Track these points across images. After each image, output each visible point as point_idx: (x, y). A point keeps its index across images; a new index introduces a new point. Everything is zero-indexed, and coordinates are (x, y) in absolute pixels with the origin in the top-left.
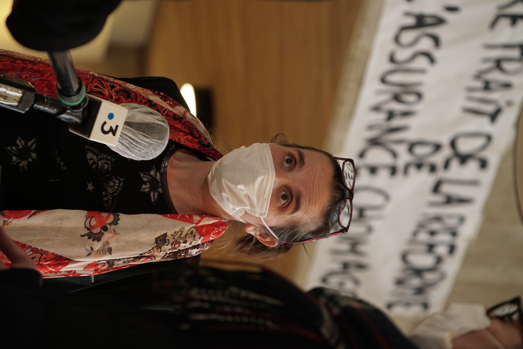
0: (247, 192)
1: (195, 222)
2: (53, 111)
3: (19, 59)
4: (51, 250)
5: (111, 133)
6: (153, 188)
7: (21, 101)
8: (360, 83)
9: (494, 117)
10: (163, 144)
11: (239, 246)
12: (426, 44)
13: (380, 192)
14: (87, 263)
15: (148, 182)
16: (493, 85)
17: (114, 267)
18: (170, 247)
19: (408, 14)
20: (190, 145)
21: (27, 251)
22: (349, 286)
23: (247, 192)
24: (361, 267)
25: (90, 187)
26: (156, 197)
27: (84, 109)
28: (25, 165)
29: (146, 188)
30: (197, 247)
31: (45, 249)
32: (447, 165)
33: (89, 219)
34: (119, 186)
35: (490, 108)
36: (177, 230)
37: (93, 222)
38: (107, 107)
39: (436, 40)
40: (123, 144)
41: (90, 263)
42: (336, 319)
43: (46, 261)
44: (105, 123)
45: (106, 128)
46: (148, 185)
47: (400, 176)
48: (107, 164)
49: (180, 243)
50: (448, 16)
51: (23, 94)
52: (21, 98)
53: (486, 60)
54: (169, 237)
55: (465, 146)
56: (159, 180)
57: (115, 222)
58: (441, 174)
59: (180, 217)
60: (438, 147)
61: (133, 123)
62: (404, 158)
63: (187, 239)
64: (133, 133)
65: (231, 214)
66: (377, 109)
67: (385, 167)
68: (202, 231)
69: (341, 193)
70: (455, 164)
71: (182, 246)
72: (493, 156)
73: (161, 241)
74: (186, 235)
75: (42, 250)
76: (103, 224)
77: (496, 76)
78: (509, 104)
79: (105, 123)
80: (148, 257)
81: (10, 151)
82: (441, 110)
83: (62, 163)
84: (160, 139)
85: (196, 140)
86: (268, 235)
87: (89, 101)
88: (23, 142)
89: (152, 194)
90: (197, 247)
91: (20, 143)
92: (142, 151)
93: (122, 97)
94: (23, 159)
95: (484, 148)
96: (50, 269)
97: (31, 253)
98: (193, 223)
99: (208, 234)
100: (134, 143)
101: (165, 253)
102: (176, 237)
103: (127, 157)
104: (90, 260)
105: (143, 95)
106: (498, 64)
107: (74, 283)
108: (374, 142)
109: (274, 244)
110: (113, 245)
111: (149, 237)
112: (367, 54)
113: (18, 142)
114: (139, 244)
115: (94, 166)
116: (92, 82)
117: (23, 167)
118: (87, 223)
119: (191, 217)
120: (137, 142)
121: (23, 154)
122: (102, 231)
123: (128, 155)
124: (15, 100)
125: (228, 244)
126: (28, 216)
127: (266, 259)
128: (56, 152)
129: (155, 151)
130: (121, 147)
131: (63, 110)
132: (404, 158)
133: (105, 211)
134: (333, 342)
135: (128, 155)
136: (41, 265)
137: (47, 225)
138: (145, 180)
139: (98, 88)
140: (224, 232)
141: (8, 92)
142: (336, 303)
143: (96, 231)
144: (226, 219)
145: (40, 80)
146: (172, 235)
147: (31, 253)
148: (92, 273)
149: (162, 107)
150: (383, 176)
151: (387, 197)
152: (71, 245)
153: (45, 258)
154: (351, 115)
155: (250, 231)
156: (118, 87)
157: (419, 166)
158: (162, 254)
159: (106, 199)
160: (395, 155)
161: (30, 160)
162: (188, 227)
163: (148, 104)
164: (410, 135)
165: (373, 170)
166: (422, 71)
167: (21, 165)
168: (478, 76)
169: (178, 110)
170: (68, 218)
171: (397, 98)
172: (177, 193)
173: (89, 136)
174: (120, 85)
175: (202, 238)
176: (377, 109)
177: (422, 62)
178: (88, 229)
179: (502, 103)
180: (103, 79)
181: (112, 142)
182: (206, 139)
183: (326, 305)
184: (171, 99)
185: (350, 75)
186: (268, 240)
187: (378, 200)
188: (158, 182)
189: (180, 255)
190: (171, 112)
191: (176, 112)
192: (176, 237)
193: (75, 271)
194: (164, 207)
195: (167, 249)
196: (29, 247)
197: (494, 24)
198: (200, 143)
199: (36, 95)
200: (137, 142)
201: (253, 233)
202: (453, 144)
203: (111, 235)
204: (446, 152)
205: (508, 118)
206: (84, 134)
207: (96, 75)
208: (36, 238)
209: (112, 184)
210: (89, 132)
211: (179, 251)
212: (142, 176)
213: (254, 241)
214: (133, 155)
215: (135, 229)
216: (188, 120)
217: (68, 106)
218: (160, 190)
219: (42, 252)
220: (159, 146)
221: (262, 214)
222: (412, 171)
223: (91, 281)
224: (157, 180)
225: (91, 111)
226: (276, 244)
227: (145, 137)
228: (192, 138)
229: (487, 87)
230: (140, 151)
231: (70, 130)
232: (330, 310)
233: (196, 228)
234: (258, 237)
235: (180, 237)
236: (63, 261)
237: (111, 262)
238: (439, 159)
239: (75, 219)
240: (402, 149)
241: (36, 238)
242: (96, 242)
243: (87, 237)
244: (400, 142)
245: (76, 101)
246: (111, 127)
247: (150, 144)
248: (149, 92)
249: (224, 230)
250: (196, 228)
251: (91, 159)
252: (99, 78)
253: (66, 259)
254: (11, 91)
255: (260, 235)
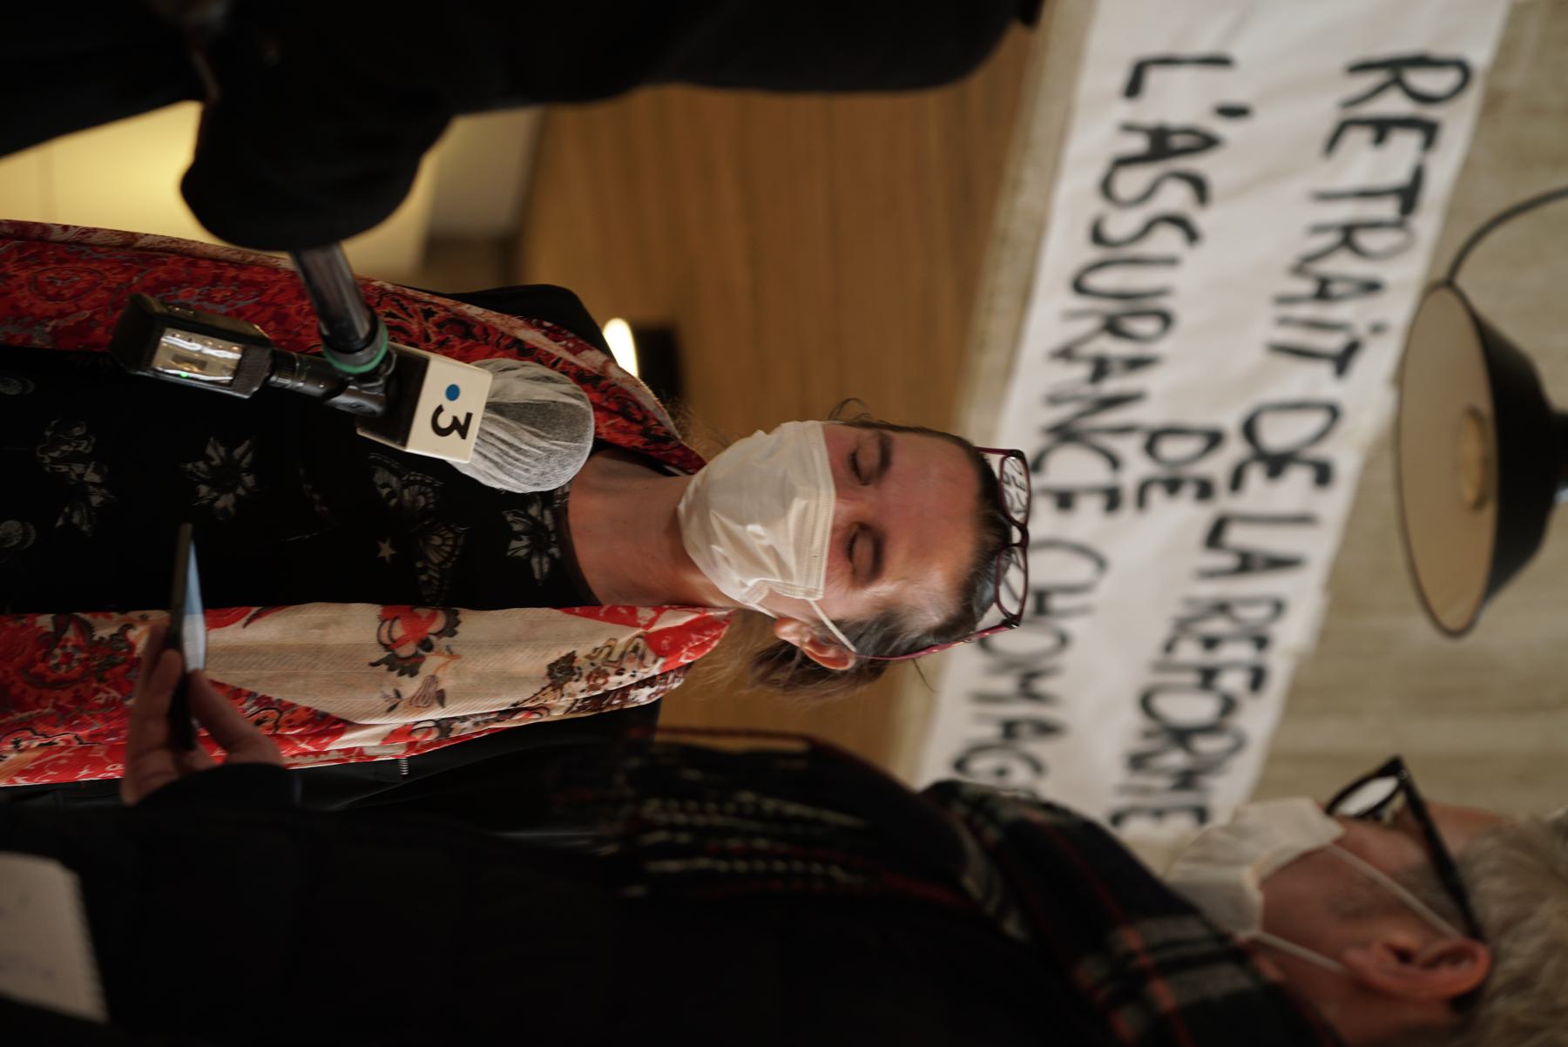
0: (772, 544)
1: (643, 622)
2: (316, 389)
3: (204, 257)
4: (303, 702)
5: (455, 434)
6: (539, 546)
7: (238, 369)
8: (1025, 296)
9: (1343, 361)
10: (580, 450)
11: (761, 670)
12: (1175, 197)
13: (1082, 550)
14: (388, 729)
15: (524, 533)
16: (1337, 289)
17: (453, 735)
18: (583, 684)
19: (1129, 128)
20: (622, 440)
21: (245, 705)
22: (1020, 776)
23: (772, 544)
24: (1046, 729)
25: (386, 551)
26: (546, 567)
27: (389, 380)
28: (230, 504)
29: (519, 547)
30: (650, 682)
31: (289, 699)
32: (1237, 480)
33: (387, 623)
34: (454, 547)
35: (1333, 342)
36: (600, 643)
37: (399, 631)
38: (441, 371)
39: (1199, 187)
40: (485, 457)
41: (395, 727)
42: (993, 854)
43: (292, 728)
44: (440, 410)
45: (444, 421)
46: (525, 541)
47: (1128, 510)
48: (424, 494)
49: (606, 675)
50: (1224, 129)
51: (244, 353)
52: (240, 361)
53: (1319, 229)
54: (581, 660)
55: (1279, 434)
56: (551, 528)
57: (450, 630)
58: (1225, 502)
59: (607, 613)
60: (1214, 439)
61: (506, 405)
62: (1137, 467)
63: (625, 665)
64: (507, 429)
65: (736, 598)
66: (1066, 354)
67: (1092, 490)
68: (661, 644)
69: (998, 534)
70: (1256, 477)
71: (614, 682)
72: (1345, 455)
73: (562, 671)
74: (622, 655)
75: (280, 701)
76: (420, 635)
77: (1343, 265)
78: (1378, 329)
79: (440, 410)
80: (532, 710)
81: (191, 473)
82: (1205, 370)
83: (316, 497)
84: (574, 440)
85: (635, 428)
86: (830, 641)
87: (399, 358)
88: (222, 450)
89: (535, 561)
90: (650, 682)
91: (216, 453)
92: (534, 471)
93: (469, 343)
94: (224, 490)
95: (1321, 436)
96: (303, 746)
97: (255, 709)
98: (638, 626)
99: (675, 649)
100: (512, 453)
101: (571, 699)
102: (598, 662)
103: (497, 486)
104: (396, 722)
105: (502, 329)
106: (1348, 236)
107: (361, 776)
108: (1064, 434)
109: (846, 664)
110: (447, 684)
111: (532, 663)
112: (1040, 227)
113: (210, 451)
114: (511, 680)
115: (393, 502)
116: (378, 305)
117: (225, 509)
118: (384, 632)
119: (633, 611)
120: (518, 450)
121: (224, 478)
122: (421, 652)
123: (501, 481)
124: (225, 368)
125: (731, 667)
126: (244, 620)
127: (827, 699)
128: (302, 471)
129: (564, 467)
130: (483, 465)
131: (340, 386)
132: (1137, 467)
133: (424, 605)
134: (991, 908)
135: (501, 481)
136: (281, 737)
137: (291, 640)
138: (517, 528)
139: (394, 316)
140: (715, 643)
141: (207, 351)
142: (991, 816)
143: (407, 650)
144: (721, 609)
145: (258, 303)
146: (588, 657)
147: (255, 709)
148: (401, 752)
149: (549, 356)
150: (1090, 507)
151: (1101, 563)
152: (350, 687)
153: (289, 721)
154: (1008, 371)
155: (787, 633)
156: (442, 314)
157: (1173, 486)
158: (565, 702)
159: (424, 578)
160: (1114, 462)
161: (240, 491)
162: (625, 636)
163: (515, 350)
164: (1147, 414)
165: (1065, 500)
166: (1171, 262)
167: (220, 504)
168: (1301, 268)
169: (589, 359)
170: (338, 623)
171: (1113, 327)
172: (594, 556)
173: (404, 444)
174: (446, 309)
175: (661, 661)
176: (1066, 354)
177: (1167, 241)
178: (386, 647)
179: (1361, 329)
180: (405, 297)
181: (461, 455)
182: (660, 424)
183: (968, 822)
184: (571, 335)
185: (1001, 279)
186: (831, 653)
187: (1080, 570)
188: (548, 533)
189: (609, 704)
190: (571, 364)
191: (583, 365)
192: (598, 662)
193: (361, 749)
194: (567, 591)
195: (578, 689)
196: (251, 695)
197: (1333, 142)
198: (645, 433)
199: (274, 355)
200: (518, 450)
201: (793, 640)
202: (1249, 429)
203: (440, 660)
204: (1236, 449)
205: (1377, 362)
206: (393, 439)
207: (389, 287)
208: (268, 673)
209: (437, 541)
210: (403, 435)
211: (607, 693)
212: (509, 518)
213: (798, 658)
214: (511, 481)
215: (499, 645)
216: (612, 381)
217: (349, 375)
218: (554, 551)
219: (283, 707)
220: (570, 455)
221: (809, 593)
222: (1156, 495)
223: (399, 770)
224: (545, 527)
225: (404, 383)
226: (851, 664)
227: (538, 436)
228: (625, 424)
229: (1323, 292)
230: (527, 471)
231: (360, 433)
232: (977, 833)
233: (648, 638)
234: (807, 648)
235: (607, 661)
236: (334, 725)
237: (444, 724)
238: (1217, 467)
239: (357, 625)
240: (1129, 448)
241: (268, 673)
242: (406, 678)
243: (384, 667)
244: (1125, 430)
245: (366, 361)
246: (455, 419)
247: (551, 453)
248: (516, 321)
249: (715, 638)
250: (648, 638)
251: (385, 485)
252: (394, 293)
253: (339, 721)
254: (213, 347)
255: (813, 643)
